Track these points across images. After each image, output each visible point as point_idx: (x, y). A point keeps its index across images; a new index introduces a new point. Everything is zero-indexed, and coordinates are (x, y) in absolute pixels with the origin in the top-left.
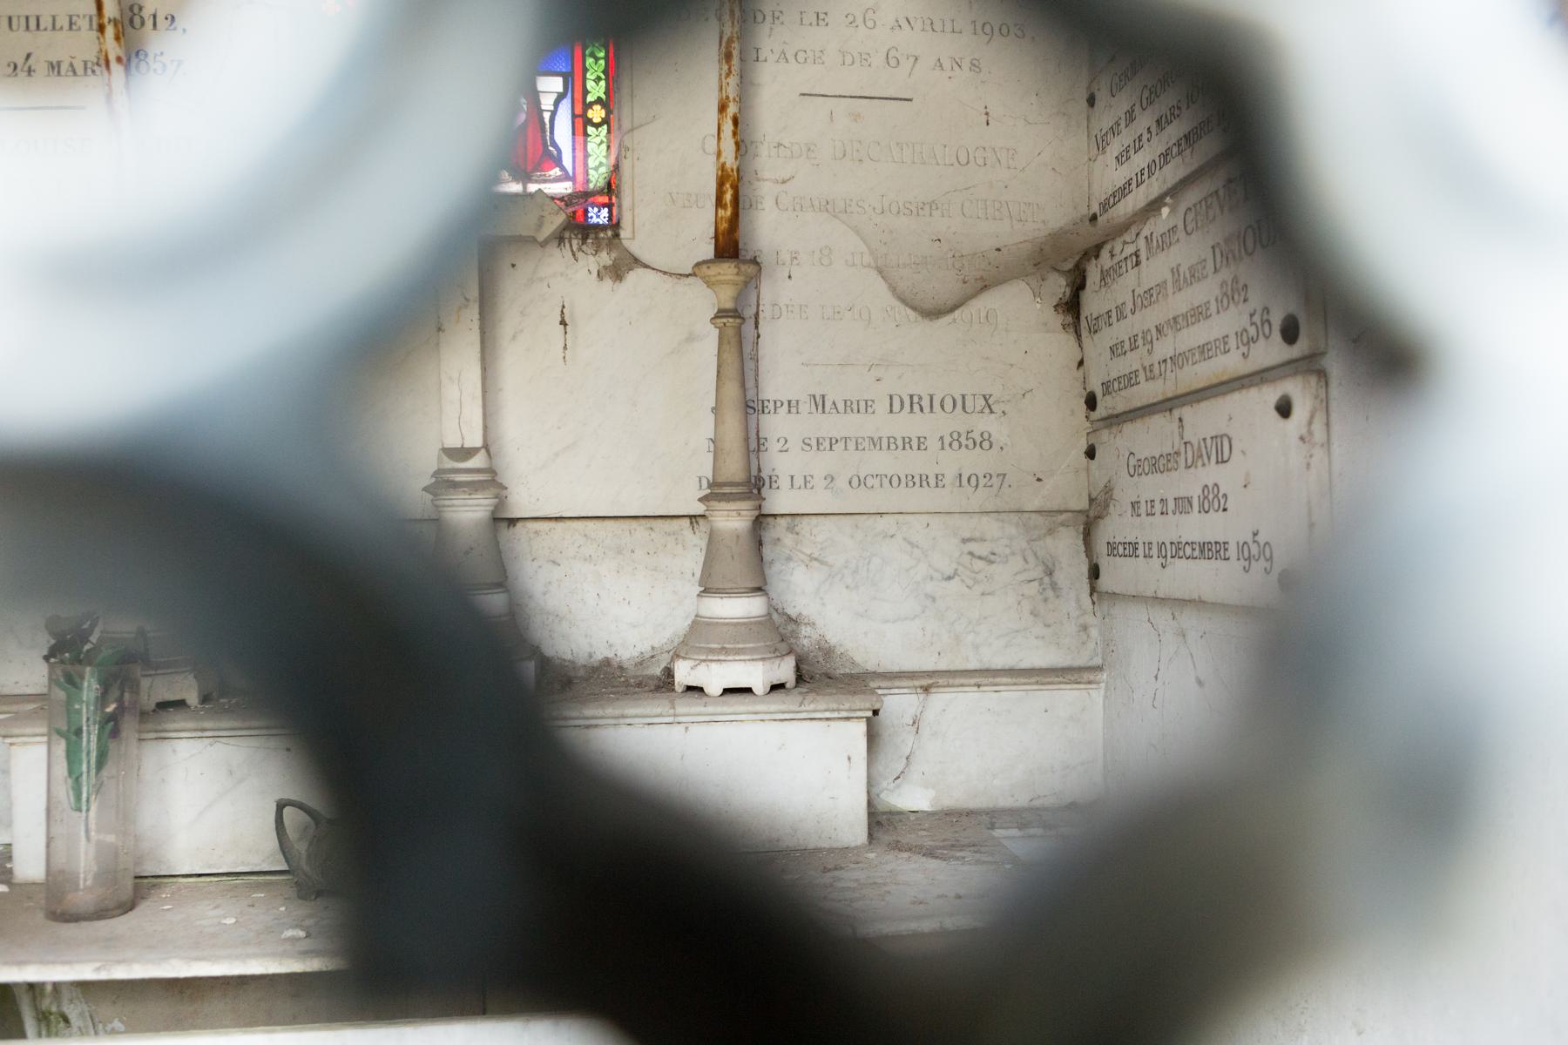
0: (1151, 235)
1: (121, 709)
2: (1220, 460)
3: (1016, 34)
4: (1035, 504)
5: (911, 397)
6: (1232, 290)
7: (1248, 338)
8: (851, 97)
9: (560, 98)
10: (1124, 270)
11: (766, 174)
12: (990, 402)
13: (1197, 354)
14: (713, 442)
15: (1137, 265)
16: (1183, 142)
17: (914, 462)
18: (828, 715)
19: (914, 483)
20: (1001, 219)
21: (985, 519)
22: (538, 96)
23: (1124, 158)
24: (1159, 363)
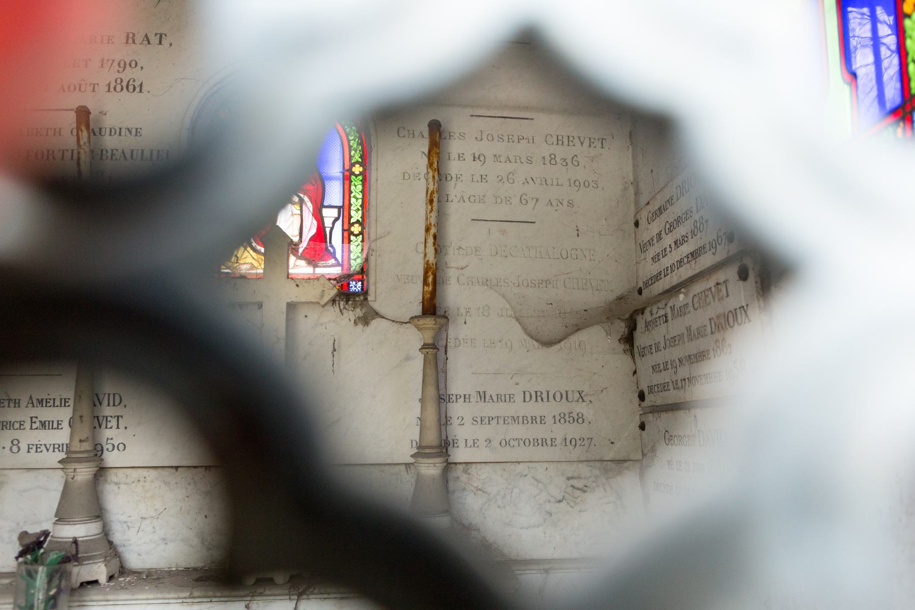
0: (674, 307)
1: (59, 591)
4: (610, 456)
5: (536, 392)
8: (501, 221)
9: (336, 220)
10: (659, 323)
11: (452, 265)
12: (583, 395)
14: (420, 420)
15: (666, 322)
16: (690, 256)
17: (538, 431)
19: (538, 444)
21: (581, 465)
22: (323, 219)
24: (681, 380)
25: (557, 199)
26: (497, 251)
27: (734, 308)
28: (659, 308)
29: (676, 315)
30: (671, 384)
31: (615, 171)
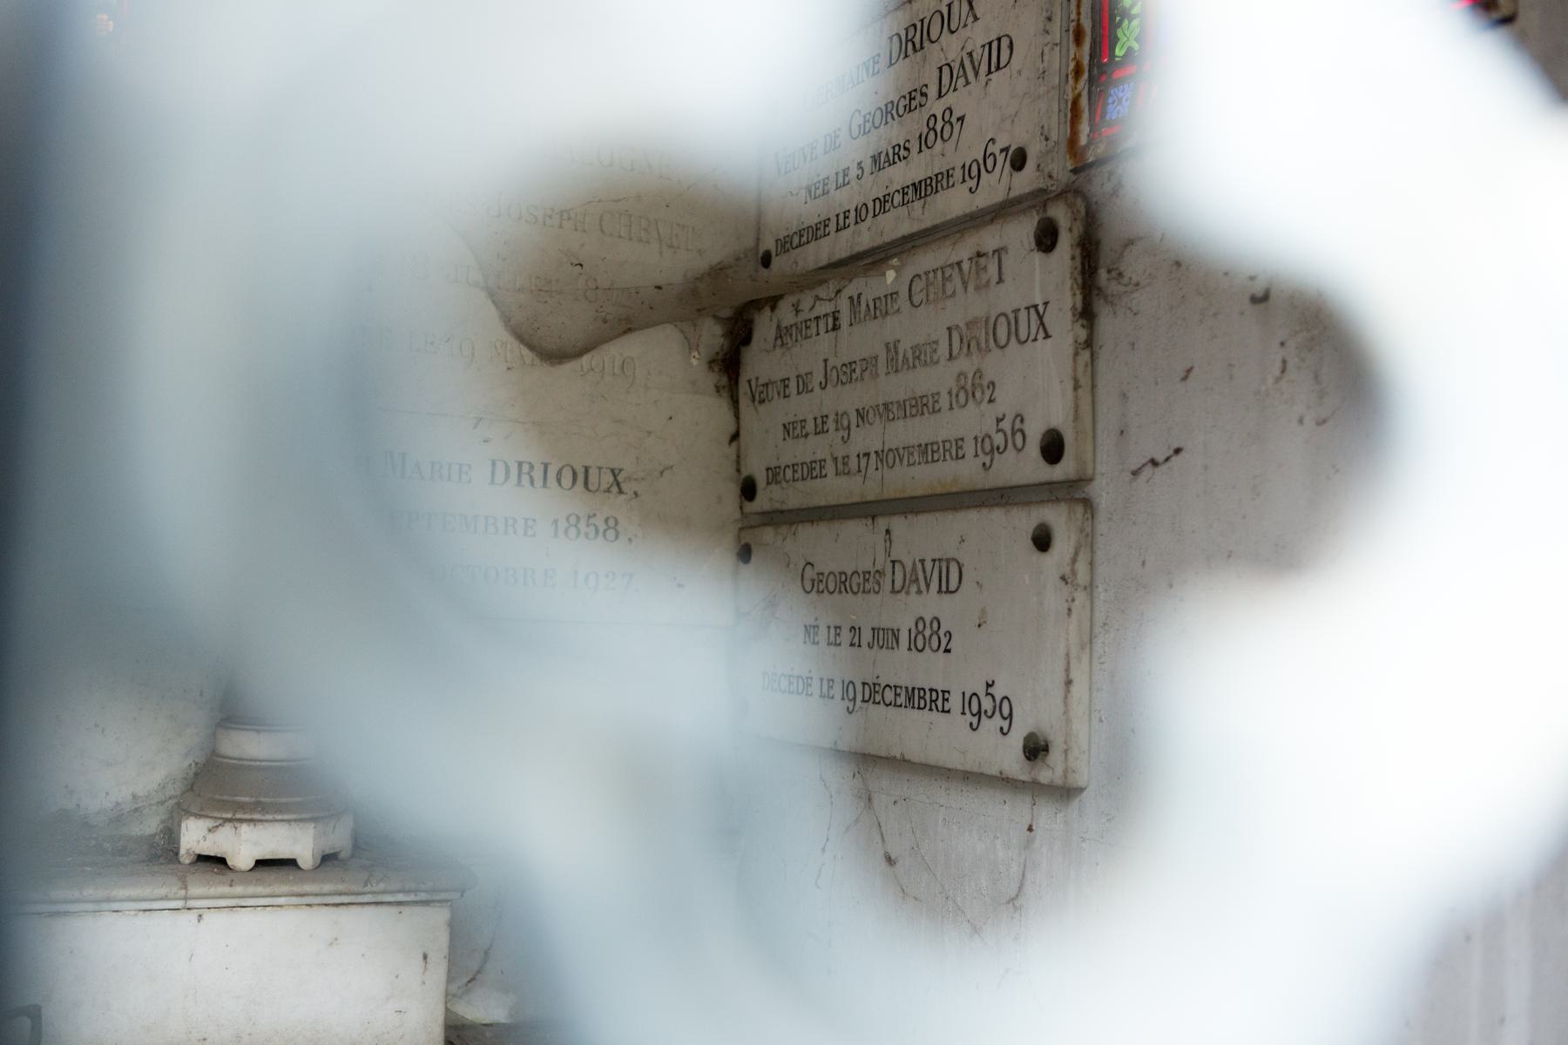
0: (859, 297)
2: (944, 588)
6: (973, 385)
7: (992, 447)
12: (620, 478)
18: (401, 897)
20: (648, 242)
27: (1015, 306)
28: (817, 298)
30: (830, 462)
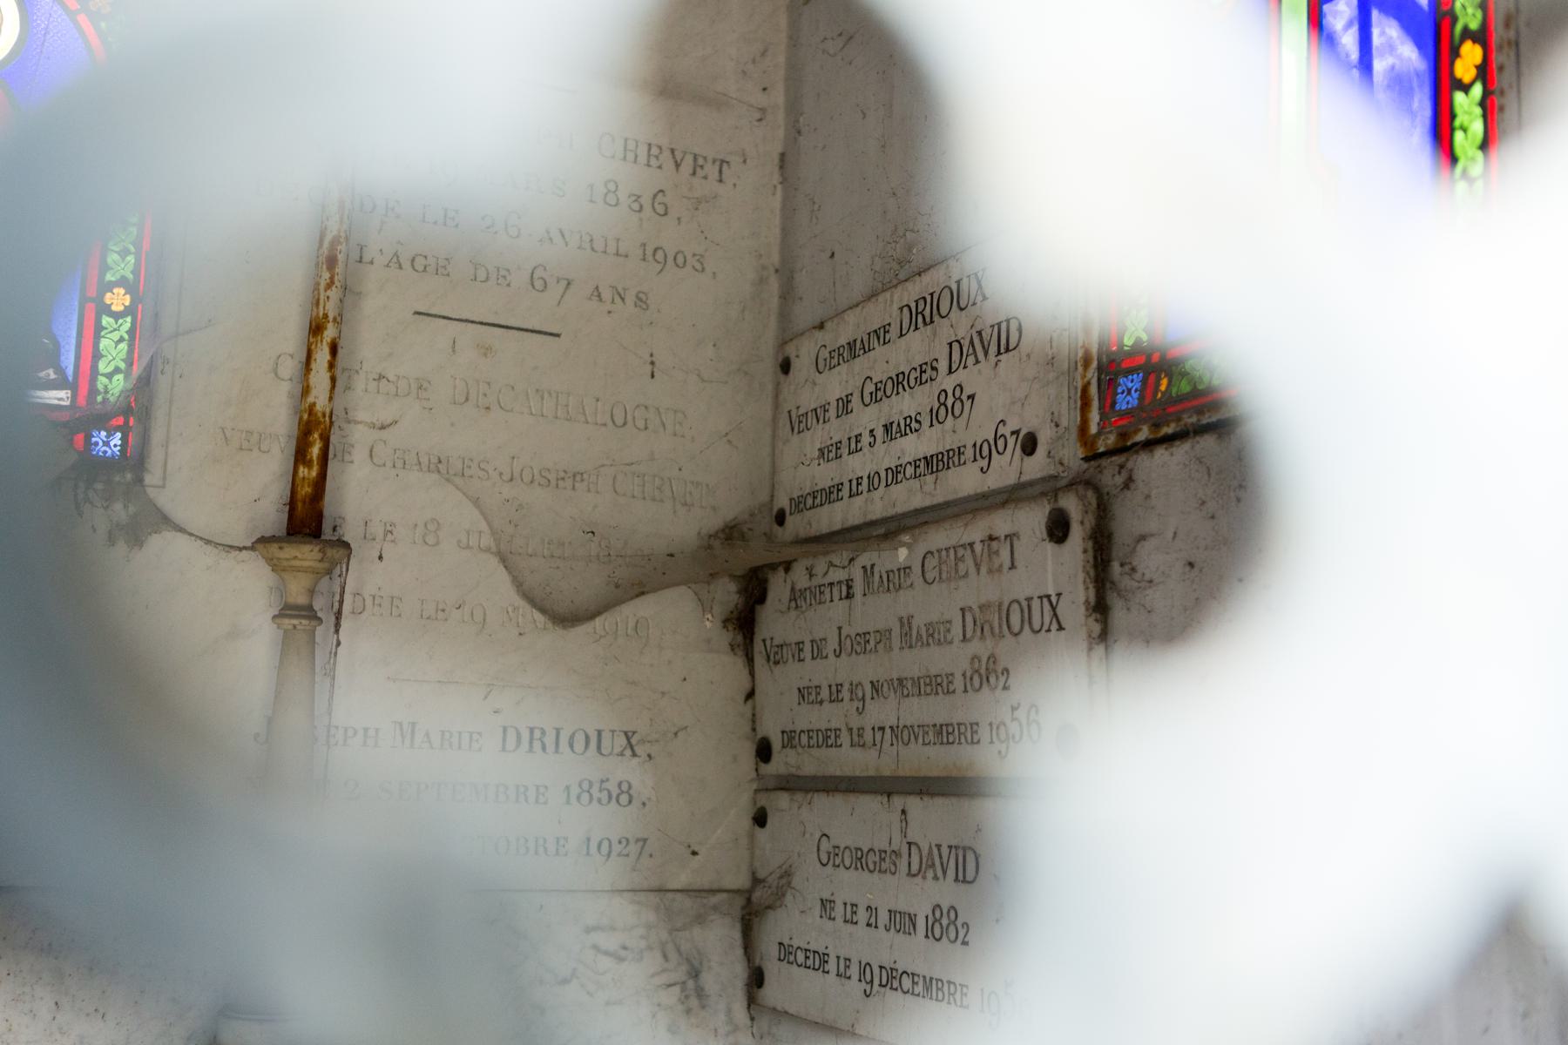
3: (693, 267)
4: (682, 879)
8: (481, 323)
11: (361, 415)
12: (633, 741)
13: (931, 733)
19: (527, 849)
20: (662, 501)
23: (832, 455)
25: (613, 287)
26: (468, 393)
28: (831, 564)
29: (876, 585)
31: (743, 238)
